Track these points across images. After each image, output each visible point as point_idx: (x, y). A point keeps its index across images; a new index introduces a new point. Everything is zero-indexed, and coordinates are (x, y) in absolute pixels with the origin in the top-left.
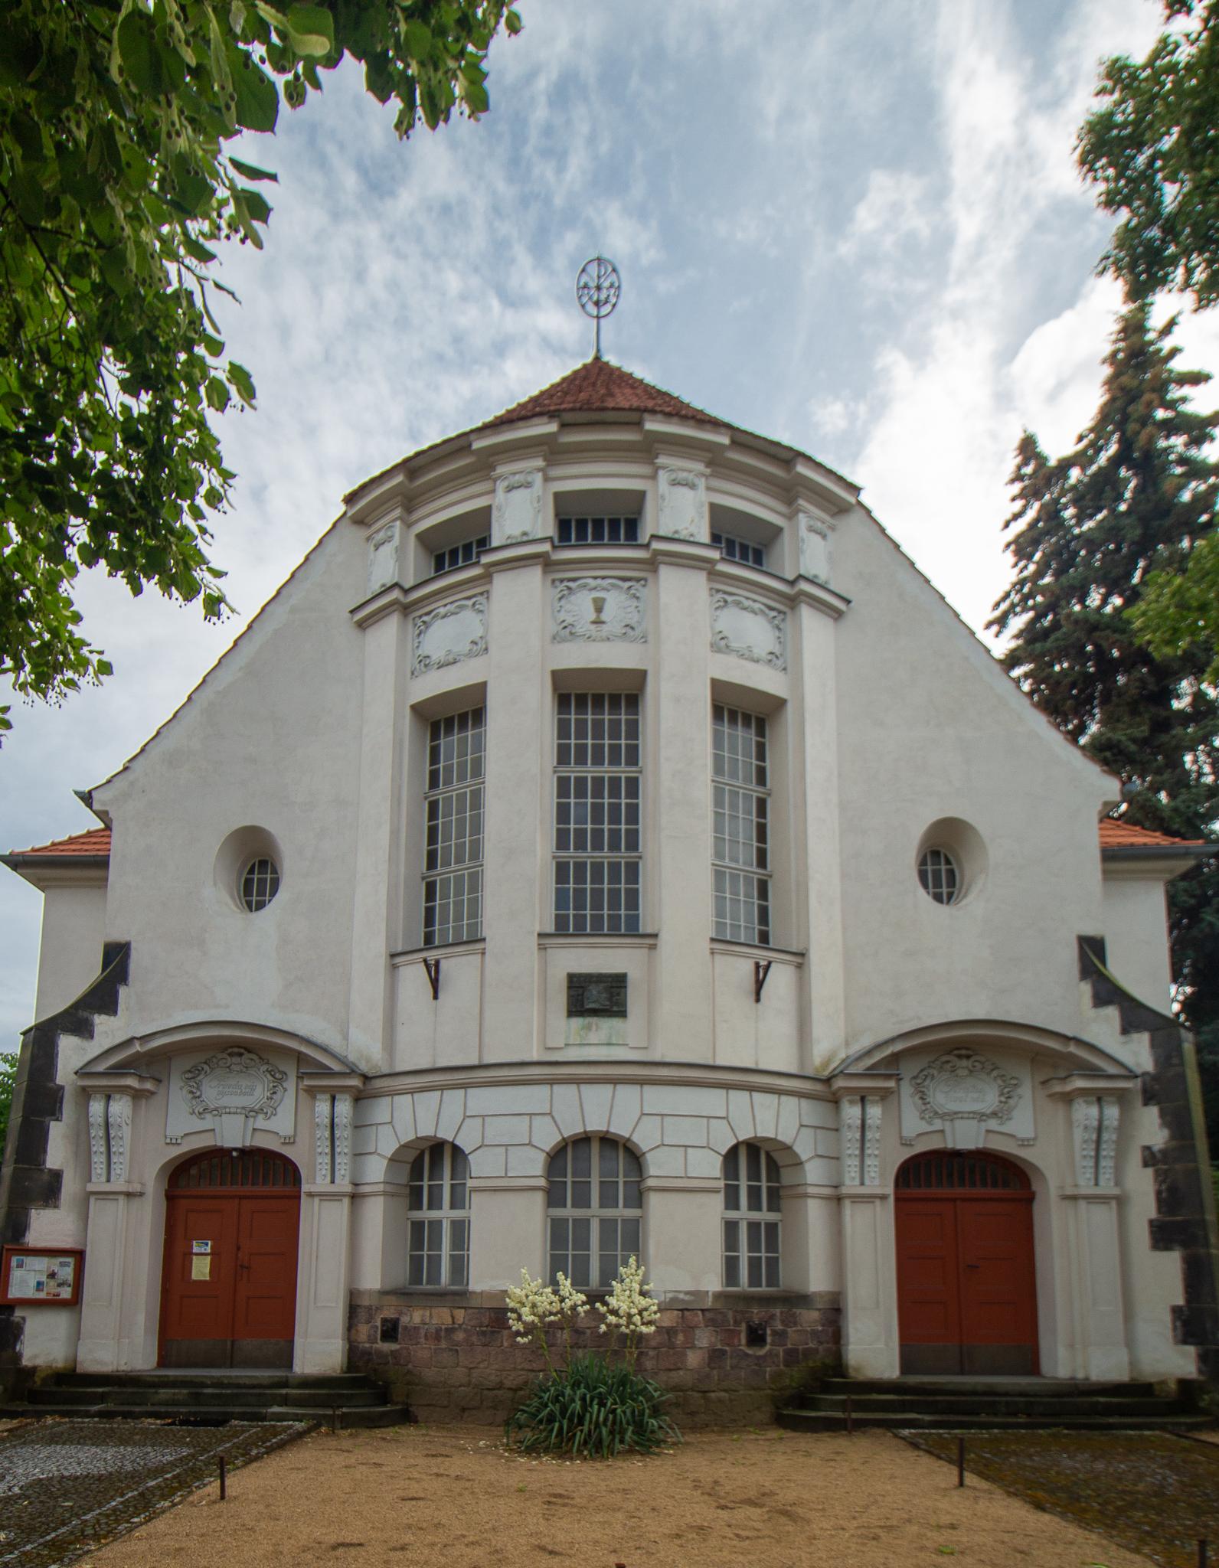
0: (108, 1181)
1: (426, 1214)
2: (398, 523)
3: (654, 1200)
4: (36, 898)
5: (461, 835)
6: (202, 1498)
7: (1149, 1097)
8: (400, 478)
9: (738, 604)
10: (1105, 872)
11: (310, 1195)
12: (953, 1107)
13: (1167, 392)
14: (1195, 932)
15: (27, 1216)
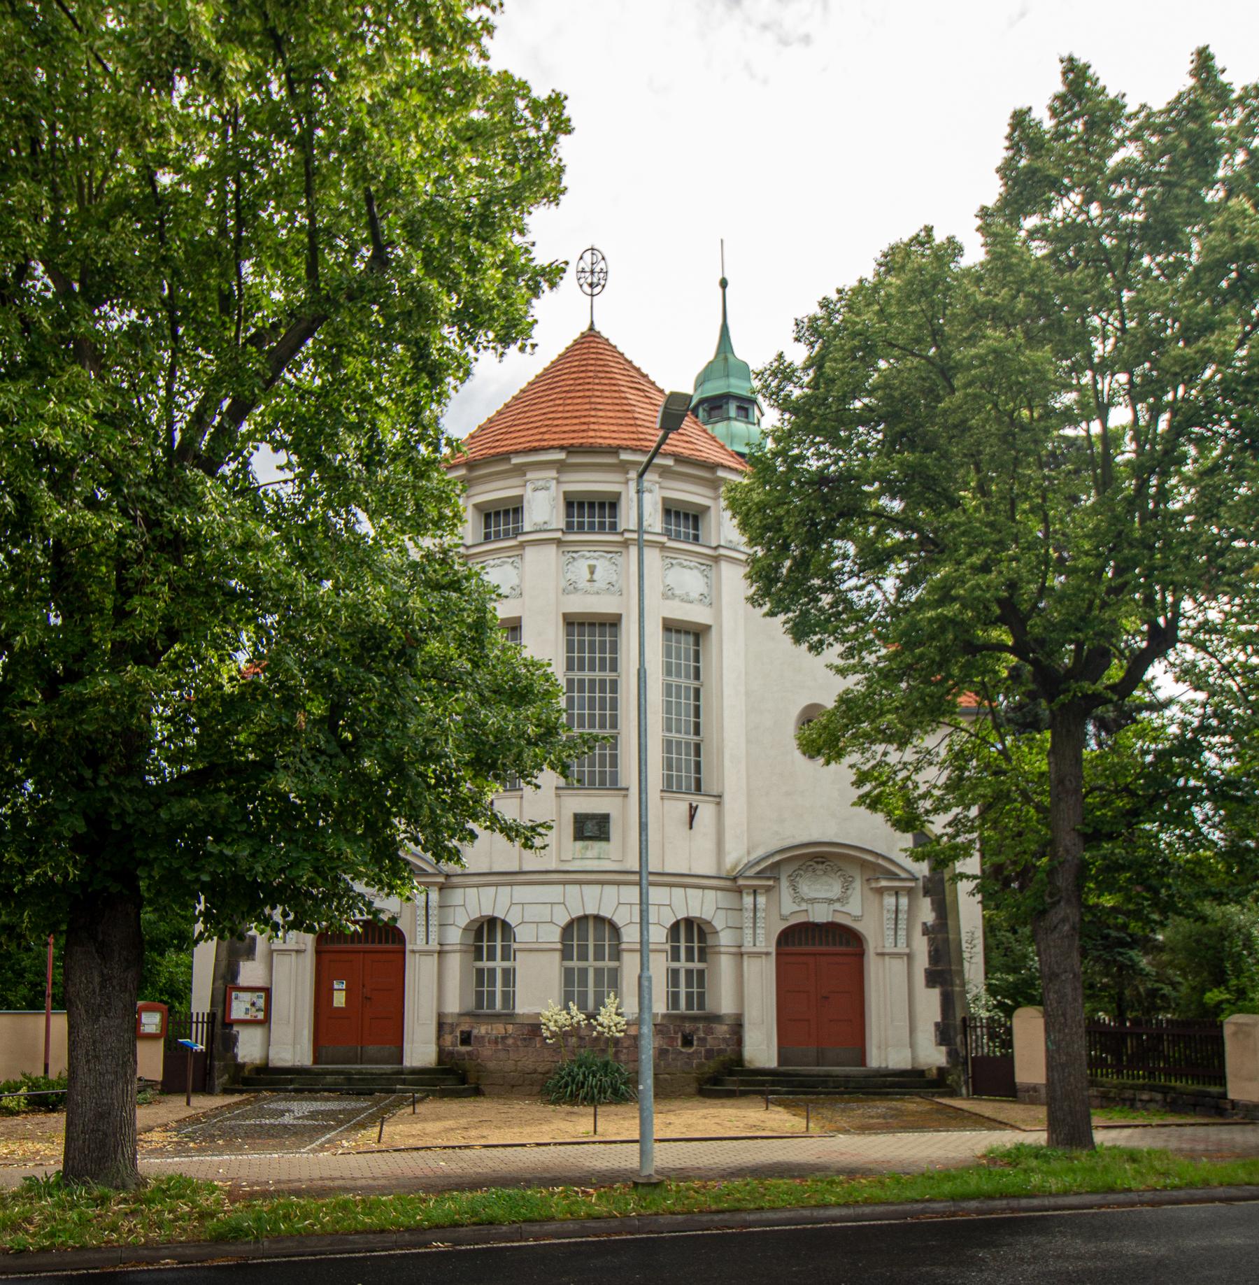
1: (486, 964)
7: (926, 893)
11: (413, 952)
12: (813, 895)
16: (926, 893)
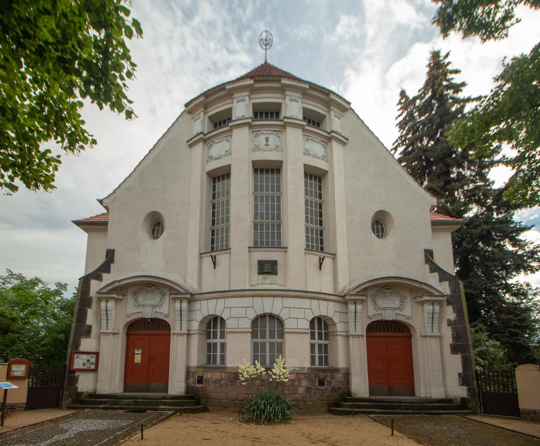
0: (107, 329)
1: (212, 341)
2: (202, 113)
3: (287, 336)
4: (86, 235)
5: (223, 214)
6: (135, 439)
7: (449, 303)
8: (202, 98)
9: (312, 140)
10: (433, 229)
11: (174, 334)
13: (447, 76)
14: (460, 249)
15: (80, 340)
16: (448, 304)
